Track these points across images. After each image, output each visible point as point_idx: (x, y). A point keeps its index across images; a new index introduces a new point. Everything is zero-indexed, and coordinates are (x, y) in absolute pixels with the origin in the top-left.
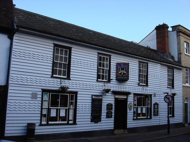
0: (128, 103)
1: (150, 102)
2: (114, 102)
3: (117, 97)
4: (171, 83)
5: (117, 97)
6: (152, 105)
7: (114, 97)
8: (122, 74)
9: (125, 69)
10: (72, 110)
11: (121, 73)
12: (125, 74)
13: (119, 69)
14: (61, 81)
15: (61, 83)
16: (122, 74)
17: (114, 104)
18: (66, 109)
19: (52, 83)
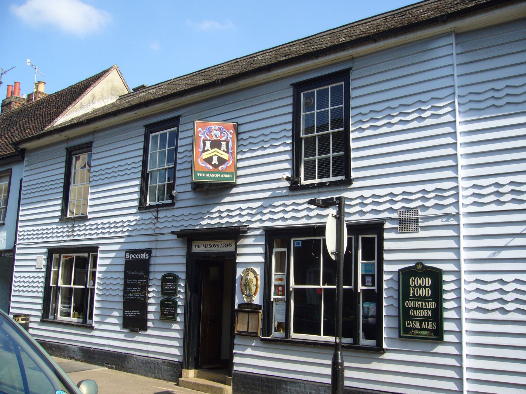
0: (239, 272)
1: (375, 261)
2: (183, 269)
3: (199, 248)
4: (324, 123)
5: (199, 248)
6: (386, 277)
7: (184, 252)
8: (215, 161)
9: (224, 144)
10: (334, 340)
11: (209, 160)
12: (226, 161)
13: (204, 144)
14: (425, 287)
15: (415, 287)
16: (215, 161)
17: (183, 276)
18: (257, 333)
19: (497, 305)
